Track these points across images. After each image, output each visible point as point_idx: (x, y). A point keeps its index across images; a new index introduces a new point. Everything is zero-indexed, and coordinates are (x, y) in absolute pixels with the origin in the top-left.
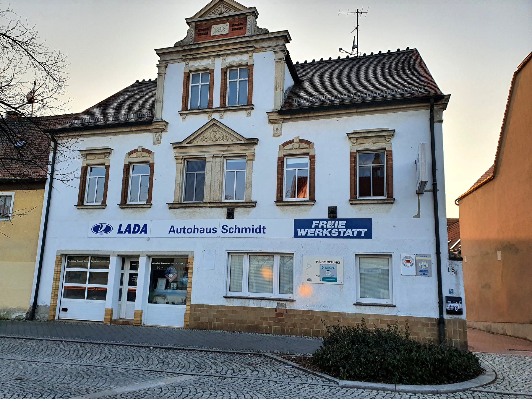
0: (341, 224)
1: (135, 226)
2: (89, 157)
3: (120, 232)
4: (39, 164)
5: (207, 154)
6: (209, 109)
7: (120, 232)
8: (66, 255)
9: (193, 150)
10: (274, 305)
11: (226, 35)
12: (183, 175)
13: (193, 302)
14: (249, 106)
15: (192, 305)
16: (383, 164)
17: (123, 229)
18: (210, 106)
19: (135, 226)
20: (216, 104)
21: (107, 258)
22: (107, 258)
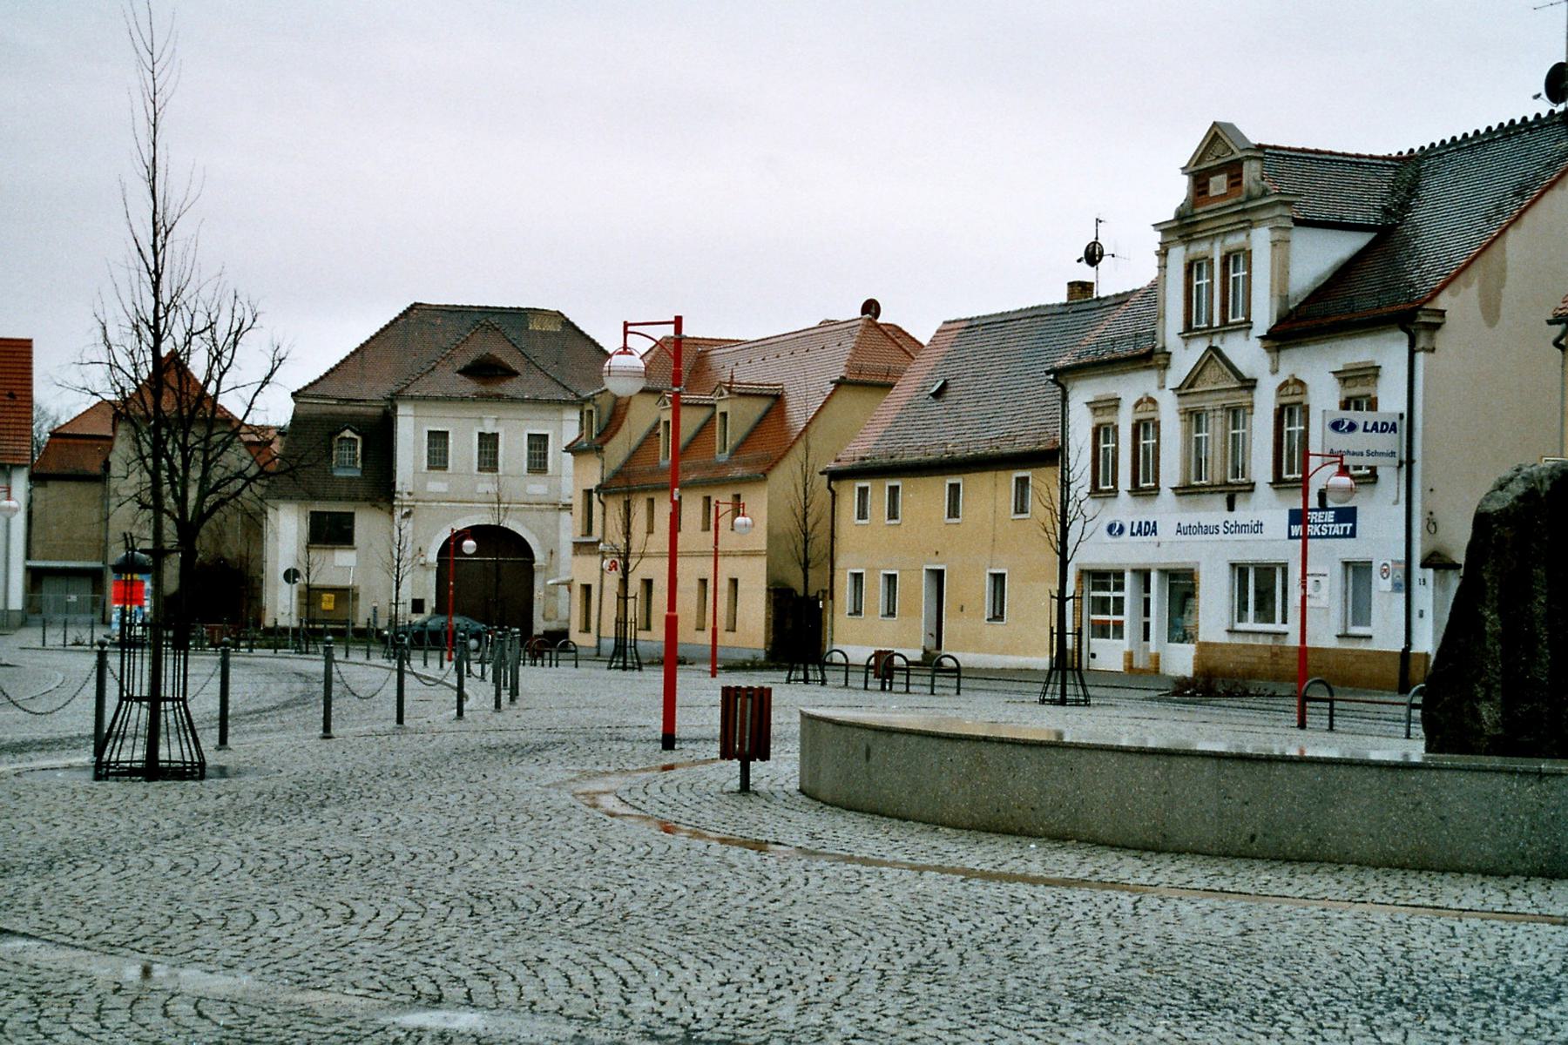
0: (1330, 516)
1: (1383, 424)
2: (1099, 413)
3: (1365, 430)
4: (189, 406)
5: (1209, 406)
6: (1210, 332)
7: (1365, 430)
8: (1089, 572)
9: (1194, 398)
10: (1269, 641)
11: (1223, 196)
12: (1226, 442)
13: (1200, 640)
14: (1247, 325)
15: (1199, 644)
16: (1094, 617)
17: (1369, 427)
18: (1210, 327)
19: (1383, 424)
20: (1216, 323)
21: (1120, 575)
22: (1120, 575)
